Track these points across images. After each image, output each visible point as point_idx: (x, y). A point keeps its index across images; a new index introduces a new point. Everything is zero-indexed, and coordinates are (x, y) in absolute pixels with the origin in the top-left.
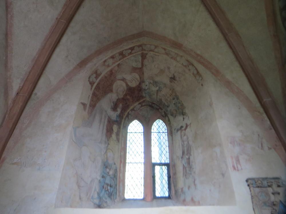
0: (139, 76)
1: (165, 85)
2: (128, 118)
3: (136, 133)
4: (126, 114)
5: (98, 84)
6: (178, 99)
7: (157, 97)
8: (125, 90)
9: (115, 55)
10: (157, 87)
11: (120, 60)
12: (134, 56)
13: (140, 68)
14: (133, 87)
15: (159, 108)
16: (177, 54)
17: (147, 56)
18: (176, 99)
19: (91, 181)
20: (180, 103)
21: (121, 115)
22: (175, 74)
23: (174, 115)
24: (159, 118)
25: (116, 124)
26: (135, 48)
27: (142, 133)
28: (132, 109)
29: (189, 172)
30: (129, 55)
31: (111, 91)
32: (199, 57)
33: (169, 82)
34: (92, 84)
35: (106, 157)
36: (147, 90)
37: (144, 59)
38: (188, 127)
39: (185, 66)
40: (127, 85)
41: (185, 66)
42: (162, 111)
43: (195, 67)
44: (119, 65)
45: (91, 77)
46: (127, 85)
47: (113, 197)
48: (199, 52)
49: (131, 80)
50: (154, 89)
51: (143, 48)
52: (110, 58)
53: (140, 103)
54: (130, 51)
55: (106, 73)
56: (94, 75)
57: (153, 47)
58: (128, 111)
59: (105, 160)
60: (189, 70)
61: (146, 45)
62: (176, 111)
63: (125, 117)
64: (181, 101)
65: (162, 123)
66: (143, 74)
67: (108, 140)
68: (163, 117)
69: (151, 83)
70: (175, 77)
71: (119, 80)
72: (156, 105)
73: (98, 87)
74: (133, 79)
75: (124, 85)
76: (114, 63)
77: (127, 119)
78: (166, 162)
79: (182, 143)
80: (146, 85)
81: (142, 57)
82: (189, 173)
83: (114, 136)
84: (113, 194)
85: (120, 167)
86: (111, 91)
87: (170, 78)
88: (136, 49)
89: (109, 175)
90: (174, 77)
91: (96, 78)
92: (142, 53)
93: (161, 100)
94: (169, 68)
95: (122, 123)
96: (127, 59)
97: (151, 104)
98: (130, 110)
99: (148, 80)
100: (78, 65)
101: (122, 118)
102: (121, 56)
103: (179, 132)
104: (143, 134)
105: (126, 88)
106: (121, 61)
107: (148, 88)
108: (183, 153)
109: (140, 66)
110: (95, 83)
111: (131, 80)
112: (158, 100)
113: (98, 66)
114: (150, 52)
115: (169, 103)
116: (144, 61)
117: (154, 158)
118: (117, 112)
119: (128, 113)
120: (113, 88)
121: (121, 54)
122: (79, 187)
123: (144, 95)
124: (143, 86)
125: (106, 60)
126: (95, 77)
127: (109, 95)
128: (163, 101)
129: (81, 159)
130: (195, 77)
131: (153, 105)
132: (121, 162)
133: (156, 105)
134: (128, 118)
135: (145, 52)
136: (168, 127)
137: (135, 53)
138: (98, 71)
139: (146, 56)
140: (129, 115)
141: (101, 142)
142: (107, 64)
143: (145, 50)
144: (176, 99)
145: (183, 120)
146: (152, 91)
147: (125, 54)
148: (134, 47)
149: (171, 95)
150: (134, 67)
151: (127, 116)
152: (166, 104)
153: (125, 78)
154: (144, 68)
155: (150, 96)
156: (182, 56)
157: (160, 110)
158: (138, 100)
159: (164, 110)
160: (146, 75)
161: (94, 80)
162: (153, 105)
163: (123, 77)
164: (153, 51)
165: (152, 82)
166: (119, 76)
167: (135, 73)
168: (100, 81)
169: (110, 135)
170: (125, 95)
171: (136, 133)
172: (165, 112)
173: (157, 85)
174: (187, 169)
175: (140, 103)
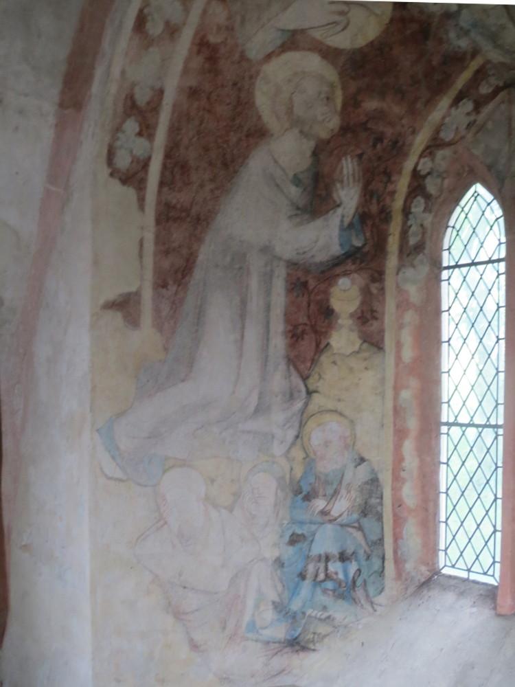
2: (428, 197)
4: (402, 184)
8: (332, 86)
27: (499, 261)
28: (428, 147)
31: (260, 133)
34: (133, 177)
40: (330, 54)
45: (118, 143)
46: (330, 54)
47: (366, 591)
49: (337, 18)
53: (457, 101)
55: (186, 71)
56: (131, 126)
58: (409, 165)
67: (305, 379)
71: (269, 57)
73: (175, 168)
74: (345, 8)
75: (313, 62)
77: (418, 205)
83: (343, 339)
84: (359, 582)
85: (399, 459)
86: (260, 133)
91: (147, 131)
98: (421, 156)
100: (62, 105)
105: (331, 74)
110: (149, 158)
111: (337, 18)
113: (123, 73)
118: (339, 211)
119: (415, 173)
120: (259, 118)
122: (178, 614)
123: (463, 43)
125: (141, 11)
126: (140, 134)
127: (257, 163)
129: (166, 523)
151: (417, 186)
153: (294, 32)
158: (438, 89)
161: (140, 146)
163: (283, 31)
166: (258, 41)
168: (174, 130)
175: (457, 101)
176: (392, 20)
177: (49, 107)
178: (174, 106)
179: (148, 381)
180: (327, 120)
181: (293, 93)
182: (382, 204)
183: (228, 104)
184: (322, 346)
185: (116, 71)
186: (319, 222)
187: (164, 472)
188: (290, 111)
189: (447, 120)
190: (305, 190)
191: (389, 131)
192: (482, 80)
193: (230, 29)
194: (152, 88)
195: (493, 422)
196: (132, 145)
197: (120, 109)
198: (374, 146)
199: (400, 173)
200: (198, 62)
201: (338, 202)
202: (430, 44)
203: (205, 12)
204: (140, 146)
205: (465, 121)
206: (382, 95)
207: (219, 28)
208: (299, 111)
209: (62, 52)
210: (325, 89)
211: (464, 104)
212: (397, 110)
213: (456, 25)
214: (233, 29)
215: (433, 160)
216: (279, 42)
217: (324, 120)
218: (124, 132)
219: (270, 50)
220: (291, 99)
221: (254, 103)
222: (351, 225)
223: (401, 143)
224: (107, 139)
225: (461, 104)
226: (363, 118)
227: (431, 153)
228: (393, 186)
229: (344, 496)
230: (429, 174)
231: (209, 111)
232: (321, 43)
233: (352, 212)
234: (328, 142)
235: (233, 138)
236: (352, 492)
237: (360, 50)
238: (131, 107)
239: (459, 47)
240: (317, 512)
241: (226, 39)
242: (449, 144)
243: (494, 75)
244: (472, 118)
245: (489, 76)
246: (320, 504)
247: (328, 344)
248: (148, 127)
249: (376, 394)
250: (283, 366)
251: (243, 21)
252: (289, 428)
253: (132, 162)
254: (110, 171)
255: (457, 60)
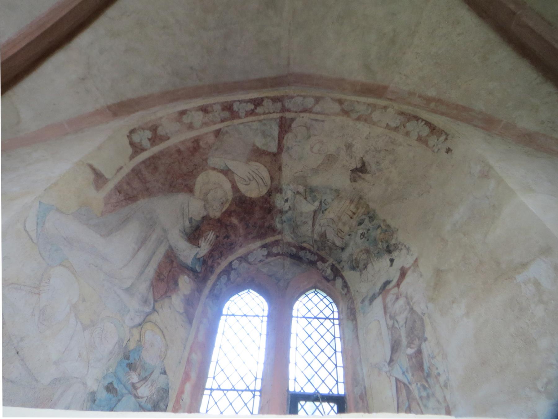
0: (270, 174)
1: (337, 193)
2: (229, 279)
3: (245, 315)
4: (224, 264)
5: (153, 158)
6: (372, 218)
7: (313, 231)
8: (227, 200)
9: (211, 105)
10: (314, 201)
11: (222, 121)
12: (260, 121)
13: (274, 155)
14: (251, 198)
15: (316, 258)
16: (374, 107)
17: (294, 125)
18: (367, 221)
19: (57, 380)
20: (379, 226)
21: (210, 262)
22: (367, 158)
23: (361, 265)
24: (315, 287)
25: (188, 276)
26: (265, 103)
28: (241, 257)
29: (424, 394)
30: (246, 116)
31: (190, 190)
32: (433, 105)
33: (348, 182)
35: (137, 337)
36: (286, 212)
37: (286, 132)
38: (409, 273)
39: (396, 129)
40: (235, 188)
41: (396, 129)
42: (326, 265)
43: (423, 120)
44: (218, 133)
46: (235, 188)
48: (431, 93)
49: (247, 179)
50: (307, 207)
51: (283, 106)
52: (197, 111)
53: (264, 246)
54: (251, 107)
55: (183, 142)
57: (310, 102)
58: (231, 258)
59: (132, 345)
60: (407, 134)
61: (292, 97)
62: (368, 252)
63: (221, 272)
64: (384, 221)
65: (325, 297)
66: (280, 169)
67: (155, 301)
68: (328, 280)
69: (298, 193)
70: (366, 164)
71: (214, 169)
72: (310, 251)
74: (252, 179)
75: (228, 186)
76: (205, 124)
77: (224, 279)
78: (335, 392)
79: (390, 323)
80: (286, 198)
81: (280, 127)
82: (421, 398)
85: (181, 392)
86: (190, 190)
87: (352, 171)
88: (268, 105)
89: (136, 397)
90: (363, 164)
92: (281, 118)
93: (323, 235)
94: (349, 147)
95: (210, 283)
96: (242, 123)
97: (294, 250)
98: (237, 259)
99: (292, 187)
100: (109, 107)
101: (212, 272)
102: (226, 114)
103: (378, 301)
104: (265, 319)
105: (230, 196)
106: (225, 124)
107: (290, 208)
108: (395, 347)
109: (273, 148)
110: (146, 150)
111: (247, 179)
112: (316, 237)
114: (302, 115)
115: (347, 237)
116: (285, 138)
117: (295, 380)
118: (198, 249)
119: (231, 264)
120: (194, 185)
121: (228, 107)
123: (279, 226)
124: (279, 201)
125: (186, 110)
127: (181, 198)
128: (331, 236)
130: (426, 143)
131: (302, 254)
132: (187, 377)
133: (310, 251)
134: (229, 279)
135: (288, 115)
136: (341, 304)
137: (264, 113)
138: (160, 129)
139: (290, 126)
140: (233, 272)
141: (129, 290)
142: (189, 121)
143: (289, 111)
144: (367, 221)
145: (391, 265)
146: (302, 213)
147: (237, 110)
148: (262, 99)
149: (354, 214)
150: (258, 148)
152: (339, 243)
153: (230, 170)
154: (284, 157)
155: (294, 228)
156: (385, 108)
157: (319, 263)
158: (261, 236)
159: (331, 261)
160: (287, 173)
161: (146, 143)
162: (302, 254)
164: (310, 112)
165: (301, 189)
166: (215, 160)
167: (258, 164)
169: (166, 292)
170: (226, 211)
171: (245, 315)
172: (333, 267)
173: (315, 196)
174: (413, 387)
175: (264, 246)
176: (263, 197)
177: (110, 102)
178: (169, 147)
179: (84, 215)
180: (216, 211)
181: (212, 189)
182: (213, 264)
183: (188, 168)
184: (168, 294)
185: (159, 114)
186: (189, 245)
187: (60, 265)
188: (206, 194)
189: (255, 252)
190: (191, 227)
191: (233, 237)
192: (276, 246)
193: (210, 147)
194: (167, 134)
195: (252, 388)
196: (143, 137)
197: (150, 125)
198: (224, 238)
199: (226, 258)
200: (190, 144)
201: (200, 245)
202: (269, 217)
203: (207, 134)
204: (146, 143)
205: (261, 258)
206: (241, 220)
207: (207, 143)
208: (210, 197)
209: (130, 95)
210: (224, 199)
211: (264, 250)
212: (241, 231)
213: (281, 217)
214: (211, 148)
215: (240, 264)
216: (222, 168)
217: (215, 210)
218: (144, 132)
219: (217, 167)
220: (210, 190)
221: (196, 178)
222: (199, 259)
223: (233, 246)
224: (136, 126)
225: (263, 249)
226: (228, 223)
227: (240, 261)
228: (221, 261)
229: (148, 386)
230: (235, 269)
231: (179, 163)
232: (235, 182)
233: (202, 255)
234: (211, 219)
235: (180, 181)
236: (154, 388)
237: (246, 197)
238: (154, 129)
239: (277, 226)
240: (130, 382)
241: (206, 148)
242: (249, 263)
243: (281, 247)
244: (264, 259)
245: (279, 246)
246: (135, 378)
247: (170, 296)
248: (154, 141)
249: (182, 343)
250: (148, 283)
251: (216, 149)
252: (138, 315)
253: (139, 143)
254: (128, 135)
255: (273, 230)
